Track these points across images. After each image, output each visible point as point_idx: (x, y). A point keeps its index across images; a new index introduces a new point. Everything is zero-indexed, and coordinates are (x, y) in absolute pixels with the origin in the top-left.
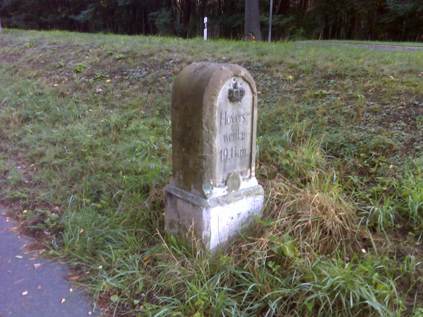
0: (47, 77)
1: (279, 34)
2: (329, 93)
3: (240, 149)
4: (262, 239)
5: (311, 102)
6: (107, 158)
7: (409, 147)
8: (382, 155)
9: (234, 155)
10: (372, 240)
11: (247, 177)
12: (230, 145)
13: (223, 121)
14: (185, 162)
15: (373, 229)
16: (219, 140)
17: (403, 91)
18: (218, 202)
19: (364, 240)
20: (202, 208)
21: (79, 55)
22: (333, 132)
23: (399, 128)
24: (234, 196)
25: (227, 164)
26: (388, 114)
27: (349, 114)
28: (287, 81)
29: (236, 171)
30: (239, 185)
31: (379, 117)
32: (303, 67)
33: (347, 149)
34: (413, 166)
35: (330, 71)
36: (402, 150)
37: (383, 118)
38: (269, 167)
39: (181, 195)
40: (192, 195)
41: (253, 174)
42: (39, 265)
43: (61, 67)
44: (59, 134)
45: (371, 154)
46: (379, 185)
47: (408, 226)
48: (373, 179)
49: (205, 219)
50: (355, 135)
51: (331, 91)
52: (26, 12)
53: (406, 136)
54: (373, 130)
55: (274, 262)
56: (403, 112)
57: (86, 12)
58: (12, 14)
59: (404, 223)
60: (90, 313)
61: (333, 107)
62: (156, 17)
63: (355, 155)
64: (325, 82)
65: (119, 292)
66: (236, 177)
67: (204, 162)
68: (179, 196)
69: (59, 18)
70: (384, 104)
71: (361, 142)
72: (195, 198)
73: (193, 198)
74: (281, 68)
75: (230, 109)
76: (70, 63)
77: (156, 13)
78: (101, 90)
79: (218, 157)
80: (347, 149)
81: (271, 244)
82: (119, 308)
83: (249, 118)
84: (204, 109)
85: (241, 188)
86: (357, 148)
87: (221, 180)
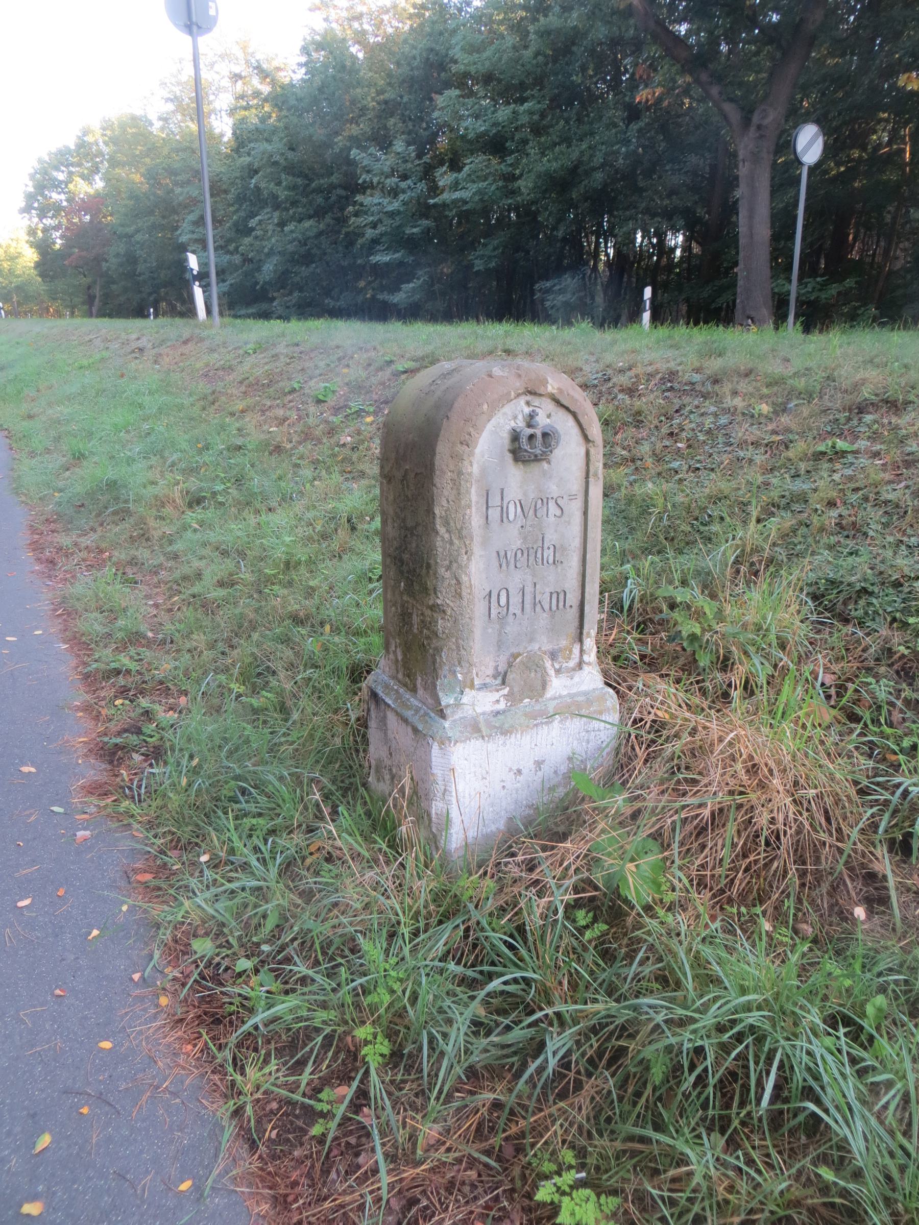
0: (263, 412)
1: (815, 317)
2: (855, 447)
3: (548, 590)
4: (568, 845)
5: (802, 472)
6: (310, 592)
9: (528, 606)
10: (891, 883)
11: (572, 664)
12: (517, 579)
13: (494, 514)
14: (405, 616)
18: (475, 729)
19: (871, 877)
20: (430, 741)
21: (332, 365)
24: (526, 715)
25: (508, 629)
27: (897, 506)
28: (753, 416)
29: (535, 646)
30: (544, 685)
32: (800, 383)
33: (874, 601)
35: (866, 393)
38: (645, 640)
39: (395, 700)
40: (416, 703)
41: (591, 656)
42: (87, 833)
43: (293, 391)
44: (239, 534)
49: (437, 771)
51: (862, 444)
52: (301, 290)
55: (591, 915)
57: (411, 285)
58: (275, 294)
60: (136, 977)
61: (857, 485)
62: (548, 291)
63: (894, 620)
64: (849, 419)
65: (218, 932)
66: (533, 665)
67: (440, 622)
68: (390, 702)
69: (360, 299)
72: (422, 712)
73: (417, 710)
74: (744, 386)
75: (515, 481)
76: (312, 383)
77: (548, 284)
78: (349, 439)
79: (480, 608)
80: (874, 601)
81: (591, 861)
82: (206, 972)
83: (575, 508)
84: (437, 480)
85: (550, 693)
86: (904, 601)
87: (490, 671)
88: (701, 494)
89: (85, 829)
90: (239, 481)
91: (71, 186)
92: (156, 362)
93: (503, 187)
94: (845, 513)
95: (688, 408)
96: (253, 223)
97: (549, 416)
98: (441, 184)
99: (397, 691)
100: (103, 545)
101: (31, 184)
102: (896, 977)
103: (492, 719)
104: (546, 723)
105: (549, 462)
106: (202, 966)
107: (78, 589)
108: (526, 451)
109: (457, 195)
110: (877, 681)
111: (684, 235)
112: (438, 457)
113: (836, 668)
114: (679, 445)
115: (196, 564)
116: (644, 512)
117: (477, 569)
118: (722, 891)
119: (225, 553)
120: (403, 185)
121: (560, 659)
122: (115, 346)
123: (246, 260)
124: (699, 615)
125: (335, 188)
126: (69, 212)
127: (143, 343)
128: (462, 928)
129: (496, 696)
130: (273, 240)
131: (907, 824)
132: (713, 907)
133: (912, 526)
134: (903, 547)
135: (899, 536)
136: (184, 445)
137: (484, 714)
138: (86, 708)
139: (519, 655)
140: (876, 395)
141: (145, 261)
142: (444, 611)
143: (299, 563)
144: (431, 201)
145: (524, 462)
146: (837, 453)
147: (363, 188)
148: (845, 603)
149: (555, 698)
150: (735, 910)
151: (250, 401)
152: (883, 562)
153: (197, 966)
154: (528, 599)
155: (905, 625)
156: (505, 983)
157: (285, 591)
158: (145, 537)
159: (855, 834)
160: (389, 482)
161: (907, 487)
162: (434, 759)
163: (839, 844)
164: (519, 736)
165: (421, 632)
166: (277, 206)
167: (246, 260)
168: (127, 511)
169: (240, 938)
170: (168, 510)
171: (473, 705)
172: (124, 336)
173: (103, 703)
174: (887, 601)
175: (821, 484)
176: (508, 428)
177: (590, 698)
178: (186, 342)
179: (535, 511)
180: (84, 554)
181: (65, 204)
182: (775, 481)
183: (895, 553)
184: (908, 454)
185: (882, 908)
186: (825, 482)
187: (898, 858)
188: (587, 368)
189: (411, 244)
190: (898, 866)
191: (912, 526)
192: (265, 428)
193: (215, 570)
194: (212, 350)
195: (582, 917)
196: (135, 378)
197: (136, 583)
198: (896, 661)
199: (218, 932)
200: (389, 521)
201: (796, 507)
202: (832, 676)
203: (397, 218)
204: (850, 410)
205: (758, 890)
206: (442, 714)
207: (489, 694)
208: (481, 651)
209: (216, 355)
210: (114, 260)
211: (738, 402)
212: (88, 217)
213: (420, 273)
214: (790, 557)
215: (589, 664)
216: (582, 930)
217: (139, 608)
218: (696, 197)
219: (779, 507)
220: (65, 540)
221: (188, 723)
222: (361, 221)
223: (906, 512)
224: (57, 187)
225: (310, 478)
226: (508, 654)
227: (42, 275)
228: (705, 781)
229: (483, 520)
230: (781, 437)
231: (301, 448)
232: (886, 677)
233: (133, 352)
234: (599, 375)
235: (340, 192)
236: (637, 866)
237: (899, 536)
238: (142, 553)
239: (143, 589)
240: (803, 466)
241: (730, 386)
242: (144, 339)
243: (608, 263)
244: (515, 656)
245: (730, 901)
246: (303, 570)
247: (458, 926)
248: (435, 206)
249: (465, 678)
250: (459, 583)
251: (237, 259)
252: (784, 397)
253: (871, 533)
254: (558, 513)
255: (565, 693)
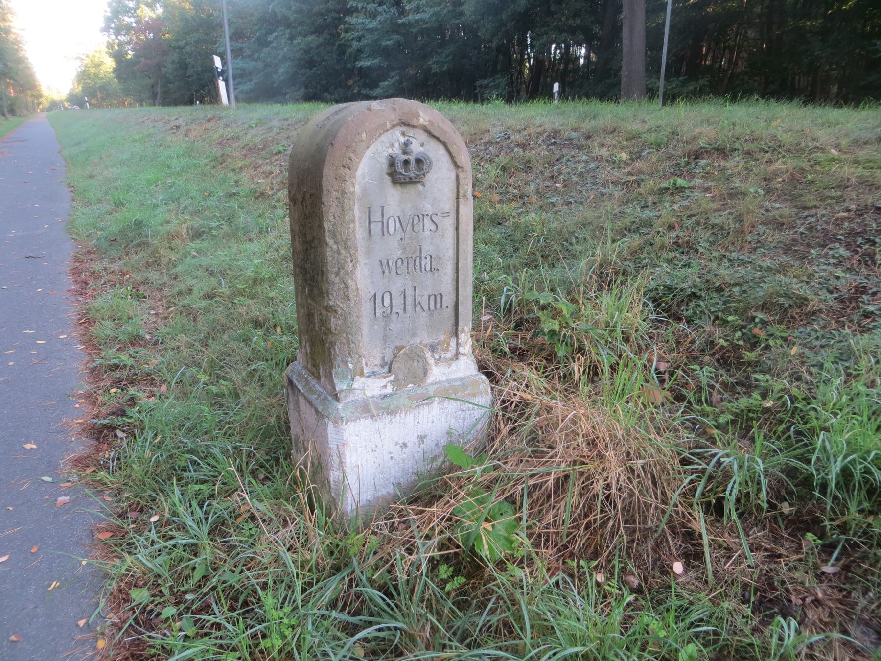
0: (256, 168)
2: (692, 184)
3: (426, 293)
5: (650, 204)
7: (851, 307)
8: (780, 323)
9: (409, 307)
10: (705, 541)
11: (449, 355)
12: (398, 284)
13: (376, 228)
14: (310, 316)
15: (716, 509)
16: (366, 272)
17: (853, 180)
18: (366, 409)
22: (680, 264)
23: (832, 261)
24: (409, 397)
25: (392, 326)
26: (811, 228)
27: (722, 228)
30: (425, 373)
31: (788, 235)
32: (652, 137)
33: (701, 303)
34: (845, 355)
35: (702, 143)
36: (830, 311)
37: (798, 237)
39: (304, 387)
40: (319, 389)
43: (280, 152)
45: (753, 318)
46: (756, 395)
47: (810, 512)
48: (748, 377)
49: (332, 445)
50: (725, 272)
53: (846, 281)
54: (768, 263)
55: (451, 569)
56: (846, 224)
57: (386, 83)
59: (797, 506)
60: (82, 623)
61: (692, 212)
63: (717, 318)
64: (688, 163)
65: (155, 583)
66: (415, 355)
68: (300, 388)
70: (805, 208)
71: (736, 290)
72: (323, 396)
74: (609, 140)
75: (394, 200)
79: (366, 308)
80: (701, 303)
81: (451, 521)
83: (448, 224)
84: (324, 199)
85: (430, 380)
86: (725, 303)
87: (378, 362)
88: (570, 222)
89: (65, 495)
90: (230, 220)
91: (138, 12)
92: (186, 135)
93: (453, 11)
94: (681, 234)
95: (566, 158)
96: (270, 38)
97: (422, 145)
98: (407, 8)
99: (306, 378)
100: (125, 270)
101: (109, 10)
102: (705, 628)
103: (380, 401)
104: (427, 404)
105: (423, 185)
106: (137, 612)
107: (99, 302)
108: (401, 174)
109: (419, 16)
110: (702, 368)
111: (586, 48)
112: (324, 179)
113: (669, 357)
114: (557, 185)
115: (190, 282)
116: (526, 236)
117: (363, 277)
118: (565, 547)
119: (212, 273)
120: (380, 9)
121: (439, 351)
122: (160, 125)
123: (267, 65)
124: (556, 314)
125: (331, 11)
126: (138, 31)
127: (181, 122)
128: (347, 580)
129: (384, 382)
130: (285, 50)
131: (720, 489)
132: (557, 561)
133: (733, 244)
134: (726, 260)
135: (723, 252)
136: (194, 193)
137: (373, 397)
138: (88, 396)
139: (402, 347)
140: (710, 145)
141: (193, 67)
142: (336, 311)
143: (263, 280)
144: (400, 21)
145: (401, 184)
146: (677, 188)
147: (350, 12)
148: (679, 305)
149: (436, 383)
150: (575, 564)
151: (247, 161)
152: (709, 272)
153: (134, 612)
154: (409, 300)
155: (725, 322)
156: (380, 630)
157: (250, 302)
158: (157, 263)
159: (675, 497)
160: (295, 204)
161: (731, 213)
162: (330, 436)
163: (663, 506)
164: (403, 415)
165: (320, 329)
166: (288, 26)
167: (267, 65)
168: (147, 244)
169: (171, 587)
170: (176, 242)
171: (363, 389)
172: (167, 117)
173: (100, 392)
174: (711, 303)
175: (663, 212)
176: (386, 154)
177: (464, 383)
178: (209, 121)
179: (413, 226)
180: (111, 277)
181: (134, 25)
182: (628, 210)
183: (719, 265)
184: (732, 189)
185: (697, 563)
186: (666, 211)
187: (712, 518)
188: (493, 130)
189: (385, 53)
190: (712, 525)
191: (733, 244)
192: (256, 180)
193: (203, 285)
194: (227, 126)
195: (444, 571)
196: (169, 147)
197: (145, 297)
198: (717, 352)
199: (155, 583)
200: (297, 237)
201: (645, 230)
202: (666, 365)
203: (376, 34)
204: (689, 157)
205: (596, 545)
206: (336, 398)
207: (378, 381)
208: (367, 341)
209: (229, 129)
210: (170, 66)
211: (604, 152)
212: (151, 35)
213: (393, 74)
214: (637, 269)
215: (464, 355)
216: (445, 582)
217: (142, 317)
218: (593, 18)
219: (630, 230)
220: (98, 266)
221: (158, 406)
222: (349, 36)
223: (728, 233)
224: (128, 12)
225: (282, 216)
226: (393, 347)
227: (119, 77)
228: (552, 453)
229: (366, 234)
230: (633, 178)
231: (279, 194)
232: (708, 365)
233: (172, 129)
234: (502, 135)
235: (334, 15)
236: (493, 526)
237: (723, 252)
238: (153, 275)
239: (149, 302)
240: (650, 199)
241: (598, 140)
242: (181, 120)
243: (531, 68)
244: (399, 349)
245: (572, 555)
246: (266, 286)
247: (344, 578)
248: (403, 24)
249: (355, 367)
250: (346, 287)
251: (260, 65)
252: (638, 147)
253: (701, 250)
254: (433, 228)
255: (444, 379)
